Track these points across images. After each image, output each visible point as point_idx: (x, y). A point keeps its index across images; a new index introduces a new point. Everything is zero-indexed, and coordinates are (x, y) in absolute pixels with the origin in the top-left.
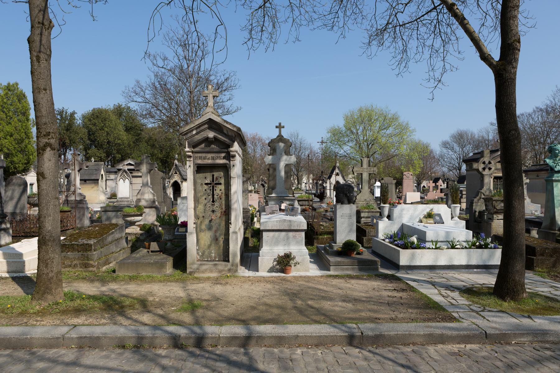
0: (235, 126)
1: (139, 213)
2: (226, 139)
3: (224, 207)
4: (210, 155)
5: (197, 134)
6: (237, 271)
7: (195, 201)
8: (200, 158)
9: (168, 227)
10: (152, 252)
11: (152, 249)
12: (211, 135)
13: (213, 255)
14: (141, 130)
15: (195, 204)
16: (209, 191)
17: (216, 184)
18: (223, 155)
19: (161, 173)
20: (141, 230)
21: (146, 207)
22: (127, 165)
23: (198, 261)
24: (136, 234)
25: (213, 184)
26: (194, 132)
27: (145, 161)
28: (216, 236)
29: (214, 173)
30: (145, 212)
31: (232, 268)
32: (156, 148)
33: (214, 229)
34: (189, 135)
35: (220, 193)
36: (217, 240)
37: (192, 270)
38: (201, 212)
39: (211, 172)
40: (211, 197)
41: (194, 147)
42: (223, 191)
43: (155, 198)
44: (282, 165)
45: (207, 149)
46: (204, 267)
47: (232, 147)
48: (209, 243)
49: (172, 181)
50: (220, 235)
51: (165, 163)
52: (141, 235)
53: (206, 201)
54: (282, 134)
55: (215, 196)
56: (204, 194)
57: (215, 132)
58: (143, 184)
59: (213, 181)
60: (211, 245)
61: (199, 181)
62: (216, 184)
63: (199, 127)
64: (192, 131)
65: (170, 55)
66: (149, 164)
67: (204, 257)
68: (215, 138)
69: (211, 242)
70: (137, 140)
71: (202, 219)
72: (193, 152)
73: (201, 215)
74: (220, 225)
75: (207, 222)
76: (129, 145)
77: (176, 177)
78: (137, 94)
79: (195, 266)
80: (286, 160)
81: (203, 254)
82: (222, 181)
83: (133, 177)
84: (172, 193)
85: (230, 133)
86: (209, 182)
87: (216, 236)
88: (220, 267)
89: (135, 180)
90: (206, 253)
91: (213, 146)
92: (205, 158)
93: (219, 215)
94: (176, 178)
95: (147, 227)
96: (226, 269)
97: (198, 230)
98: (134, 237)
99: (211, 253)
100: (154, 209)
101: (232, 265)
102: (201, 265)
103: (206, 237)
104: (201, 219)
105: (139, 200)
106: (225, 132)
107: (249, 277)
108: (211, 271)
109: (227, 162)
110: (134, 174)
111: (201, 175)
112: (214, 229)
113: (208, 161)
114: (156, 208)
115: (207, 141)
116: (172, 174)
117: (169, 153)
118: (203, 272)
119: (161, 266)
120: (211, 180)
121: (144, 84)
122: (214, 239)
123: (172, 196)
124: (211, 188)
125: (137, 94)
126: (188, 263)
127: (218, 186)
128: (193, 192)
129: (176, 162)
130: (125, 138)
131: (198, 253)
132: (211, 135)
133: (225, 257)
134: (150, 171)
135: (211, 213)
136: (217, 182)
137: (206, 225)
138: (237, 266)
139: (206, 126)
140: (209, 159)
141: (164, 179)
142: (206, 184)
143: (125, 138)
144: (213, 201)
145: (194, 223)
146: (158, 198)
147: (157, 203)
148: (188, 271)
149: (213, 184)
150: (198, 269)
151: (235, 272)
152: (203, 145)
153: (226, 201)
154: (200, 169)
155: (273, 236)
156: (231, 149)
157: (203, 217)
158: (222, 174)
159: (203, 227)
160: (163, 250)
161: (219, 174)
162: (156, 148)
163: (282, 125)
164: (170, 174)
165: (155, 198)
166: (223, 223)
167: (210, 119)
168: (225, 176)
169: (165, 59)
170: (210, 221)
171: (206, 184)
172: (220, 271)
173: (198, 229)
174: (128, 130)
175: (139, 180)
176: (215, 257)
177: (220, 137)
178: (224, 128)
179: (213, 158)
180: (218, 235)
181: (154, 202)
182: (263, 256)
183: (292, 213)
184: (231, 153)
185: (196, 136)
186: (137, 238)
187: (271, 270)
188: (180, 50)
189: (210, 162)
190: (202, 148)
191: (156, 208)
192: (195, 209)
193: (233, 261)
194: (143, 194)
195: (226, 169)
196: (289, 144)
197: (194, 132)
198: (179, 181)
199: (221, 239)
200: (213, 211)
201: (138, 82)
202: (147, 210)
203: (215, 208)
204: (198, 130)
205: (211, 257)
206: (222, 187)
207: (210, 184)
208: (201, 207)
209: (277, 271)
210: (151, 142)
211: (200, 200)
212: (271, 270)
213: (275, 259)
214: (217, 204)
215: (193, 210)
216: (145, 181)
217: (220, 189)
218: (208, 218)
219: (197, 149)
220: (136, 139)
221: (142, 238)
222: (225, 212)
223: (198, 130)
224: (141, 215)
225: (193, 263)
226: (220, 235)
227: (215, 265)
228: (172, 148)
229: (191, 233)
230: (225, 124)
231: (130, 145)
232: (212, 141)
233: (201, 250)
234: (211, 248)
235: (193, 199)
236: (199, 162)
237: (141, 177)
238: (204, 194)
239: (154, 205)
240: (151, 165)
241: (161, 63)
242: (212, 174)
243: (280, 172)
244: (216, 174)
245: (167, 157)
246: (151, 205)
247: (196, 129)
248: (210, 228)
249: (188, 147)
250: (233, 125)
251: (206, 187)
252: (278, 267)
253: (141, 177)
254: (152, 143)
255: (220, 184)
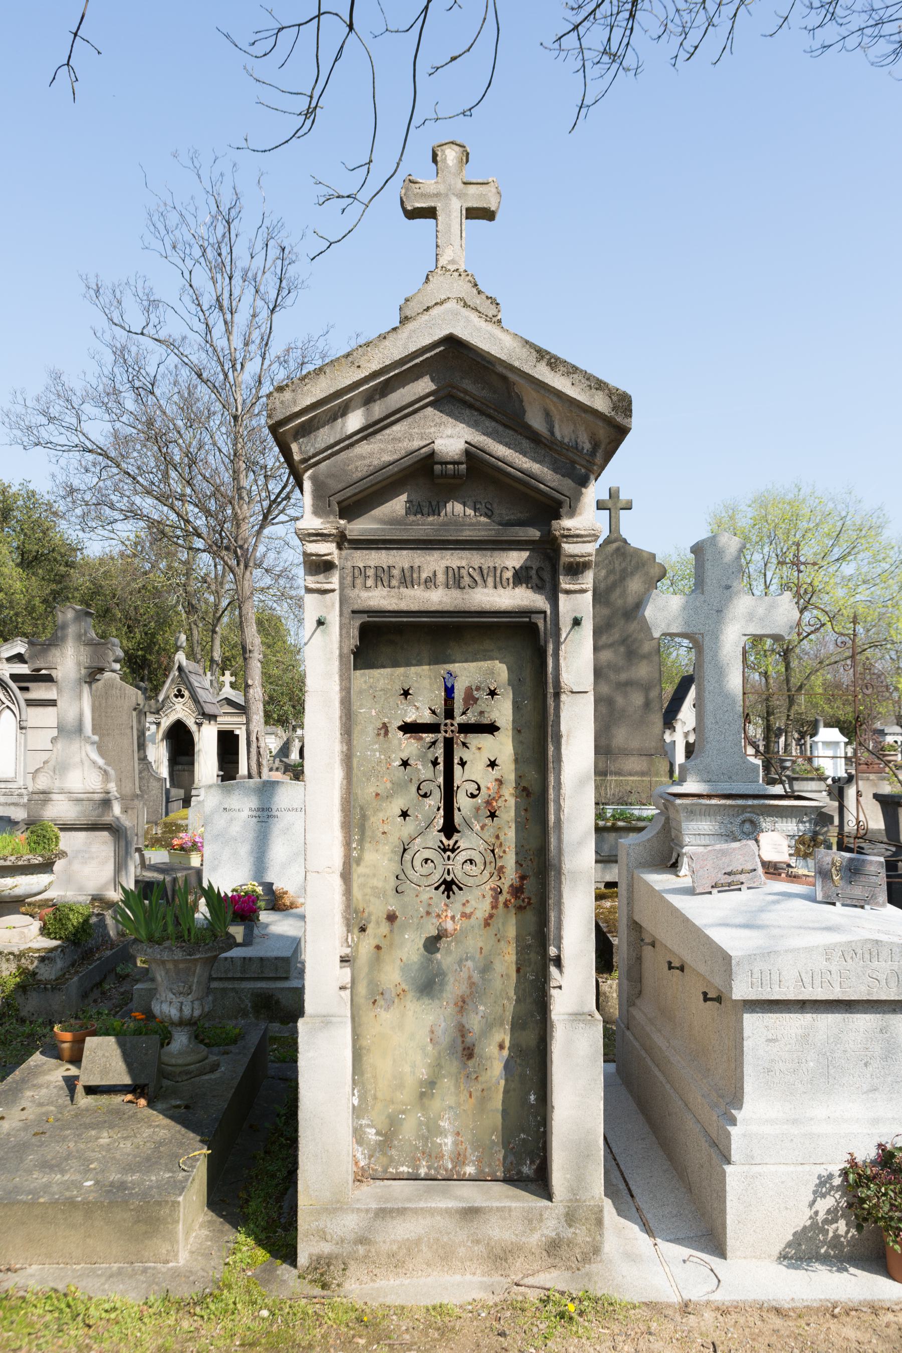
0: (600, 385)
1: (38, 860)
2: (535, 467)
3: (510, 861)
4: (435, 563)
5: (369, 431)
6: (597, 1250)
7: (347, 826)
8: (383, 576)
9: (179, 955)
10: (91, 1090)
11: (89, 1076)
12: (451, 438)
13: (447, 1143)
14: (67, 565)
15: (347, 844)
16: (425, 771)
17: (466, 729)
18: (515, 559)
19: (131, 690)
20: (45, 931)
21: (67, 828)
22: (9, 660)
23: (359, 1179)
24: (19, 957)
25: (448, 732)
26: (354, 421)
27: (72, 630)
28: (462, 1031)
29: (455, 667)
30: (63, 854)
31: (568, 1233)
32: (113, 619)
33: (454, 988)
34: (325, 436)
35: (487, 779)
36: (469, 1053)
37: (326, 1248)
38: (378, 893)
39: (438, 659)
40: (436, 800)
41: (350, 509)
42: (507, 769)
43: (112, 787)
44: (732, 639)
45: (426, 526)
46: (402, 1230)
47: (572, 513)
48: (423, 1073)
49: (166, 722)
50: (490, 1026)
51: (142, 667)
52: (46, 958)
53: (409, 828)
54: (625, 532)
55: (462, 801)
56: (399, 787)
57: (474, 425)
58: (61, 728)
59: (449, 713)
60: (432, 1084)
61: (369, 713)
62: (466, 729)
63: (385, 389)
64: (343, 411)
65: (167, 284)
66: (90, 643)
67: (387, 1157)
68: (473, 458)
69: (437, 1067)
70: (55, 594)
71: (385, 928)
72: (342, 540)
73: (377, 909)
74: (486, 969)
75: (410, 947)
76: (30, 609)
77: (178, 707)
78: (51, 420)
79: (348, 1224)
80: (751, 617)
81: (388, 1138)
82: (502, 711)
83: (31, 703)
84: (166, 763)
85: (563, 432)
86: (426, 717)
87: (462, 1031)
88: (498, 1232)
89: (35, 716)
90: (409, 1129)
91: (455, 508)
92: (408, 579)
93: (481, 906)
94: (181, 711)
95: (75, 920)
96: (535, 1239)
97: (367, 997)
98: (13, 967)
99: (431, 1130)
100: (105, 834)
101: (570, 1218)
102: (383, 1213)
103: (411, 1035)
104: (378, 930)
105: (44, 796)
106: (536, 421)
107: (686, 1308)
108: (445, 1256)
109: (538, 601)
110: (34, 695)
111: (383, 678)
112: (454, 988)
113: (429, 586)
114: (116, 830)
115: (425, 476)
116: (167, 697)
117: (153, 635)
118: (397, 1261)
119: (136, 1213)
120: (439, 705)
121: (76, 384)
122: (452, 1046)
123: (164, 772)
124: (439, 752)
125: (51, 420)
126: (303, 1201)
127: (475, 740)
128: (338, 774)
129: (181, 657)
130: (436, 1335)
131: (358, 1135)
132: (451, 438)
133: (527, 1162)
134: (93, 674)
135: (439, 897)
136: (471, 718)
137: (405, 968)
138: (599, 1222)
139: (425, 385)
140: (430, 583)
141: (141, 713)
142: (409, 728)
143: (18, 585)
144: (449, 829)
145: (344, 960)
146: (119, 781)
147: (117, 809)
148: (305, 1252)
149: (448, 732)
150: (362, 1240)
151: (586, 1259)
152: (398, 505)
153: (521, 827)
154: (378, 640)
155: (804, 1039)
156: (567, 523)
157: (391, 918)
158: (498, 671)
159: (392, 976)
160: (150, 1084)
161: (483, 674)
162: (113, 619)
163: (623, 496)
164: (161, 698)
165: (112, 787)
166: (507, 960)
167: (451, 341)
168: (516, 683)
169: (151, 304)
170: (432, 944)
171: (409, 728)
172: (500, 1257)
173: (362, 989)
174: (28, 561)
175: (45, 717)
176: (459, 1159)
177: (501, 450)
178: (530, 397)
179: (455, 580)
180: (475, 1022)
181: (106, 803)
182: (750, 1161)
183: (857, 891)
184: (568, 548)
185: (363, 448)
186: (23, 972)
187: (803, 1251)
188: (201, 278)
189: (437, 598)
190: (394, 521)
191: (116, 830)
192: (346, 876)
193: (573, 1191)
194: (61, 768)
195: (527, 642)
196: (655, 571)
197: (354, 421)
198: (190, 723)
199: (491, 1049)
200: (449, 886)
201: (57, 377)
202: (68, 841)
203: (458, 869)
204: (379, 409)
205: (434, 1155)
206: (502, 746)
207: (432, 728)
208: (379, 861)
209: (844, 1257)
210: (99, 601)
211: (375, 821)
212: (803, 1251)
213: (824, 1181)
214: (470, 843)
215: (337, 883)
216: (71, 715)
217: (489, 762)
218: (419, 927)
219: (359, 527)
220: (53, 592)
221: (47, 973)
222: (517, 891)
223: (379, 409)
224: (46, 867)
225: (335, 1208)
226: (490, 1026)
227: (470, 1213)
228: (164, 621)
229: (326, 1021)
230: (543, 373)
231: (34, 608)
232: (456, 476)
233: (377, 1116)
234: (436, 1104)
235: (337, 817)
236: (379, 598)
237: (52, 703)
238: (399, 787)
239: (107, 819)
240: (98, 645)
241: (136, 321)
242: (443, 669)
243: (721, 673)
244: (467, 673)
245: (148, 649)
246: (92, 819)
247: (368, 399)
248: (428, 985)
249: (318, 511)
250: (588, 377)
251: (409, 746)
252: (842, 1226)
253: (52, 703)
254: (103, 607)
255: (491, 729)
